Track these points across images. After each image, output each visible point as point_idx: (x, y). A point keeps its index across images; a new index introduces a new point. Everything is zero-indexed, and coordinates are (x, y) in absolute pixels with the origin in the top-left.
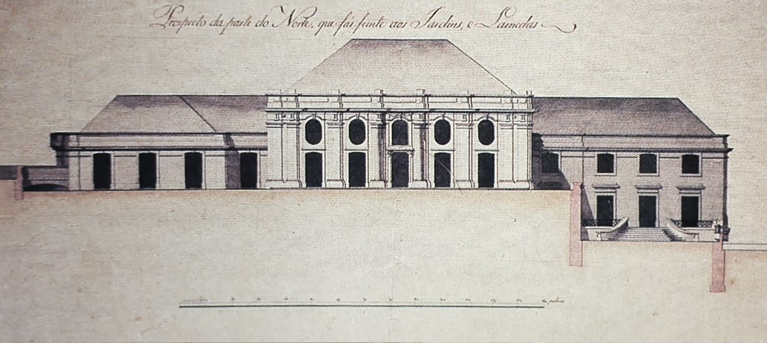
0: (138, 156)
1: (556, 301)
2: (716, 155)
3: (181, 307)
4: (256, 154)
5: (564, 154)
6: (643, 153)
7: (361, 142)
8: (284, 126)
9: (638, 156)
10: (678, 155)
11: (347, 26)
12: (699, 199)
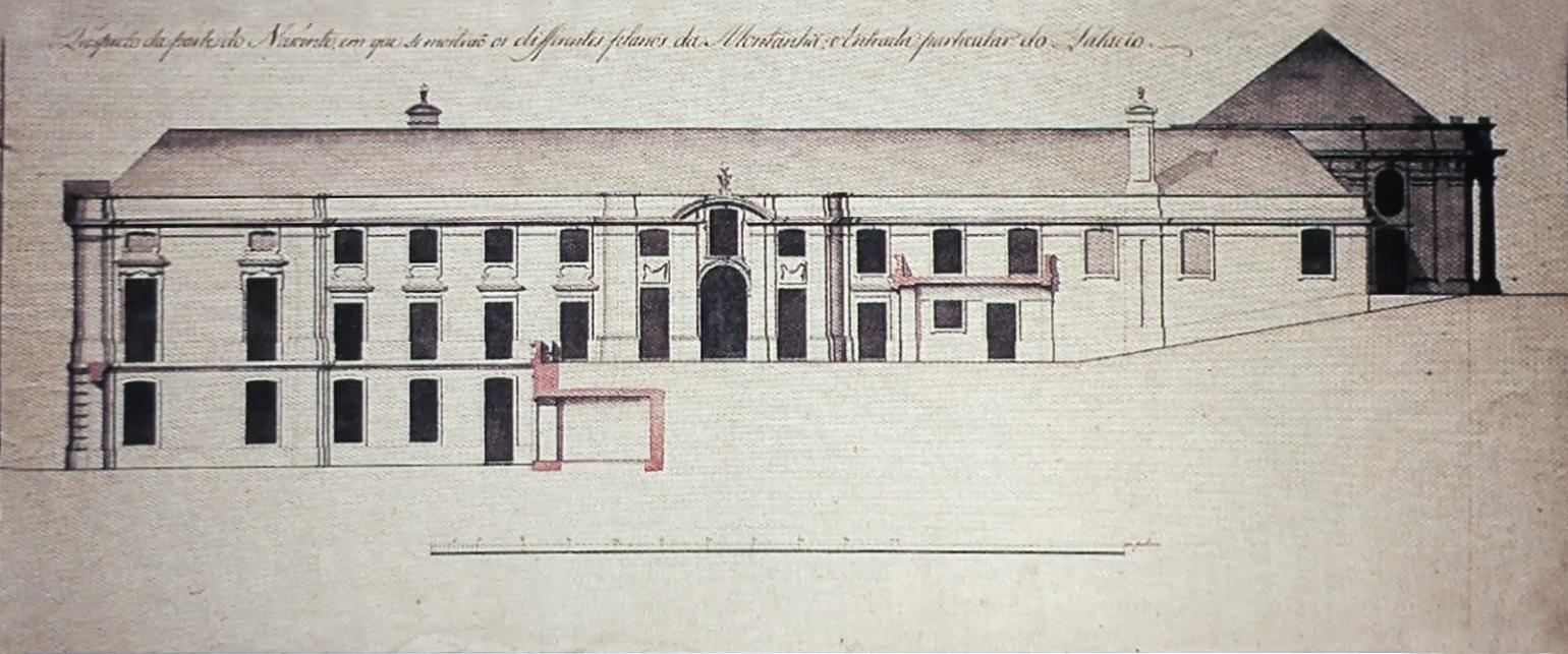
0: (559, 234)
1: (1147, 544)
2: (303, 230)
3: (433, 554)
4: (883, 232)
5: (1046, 230)
6: (492, 228)
7: (1395, 211)
8: (1441, 183)
9: (408, 233)
10: (1294, 230)
11: (778, 46)
12: (590, 305)
